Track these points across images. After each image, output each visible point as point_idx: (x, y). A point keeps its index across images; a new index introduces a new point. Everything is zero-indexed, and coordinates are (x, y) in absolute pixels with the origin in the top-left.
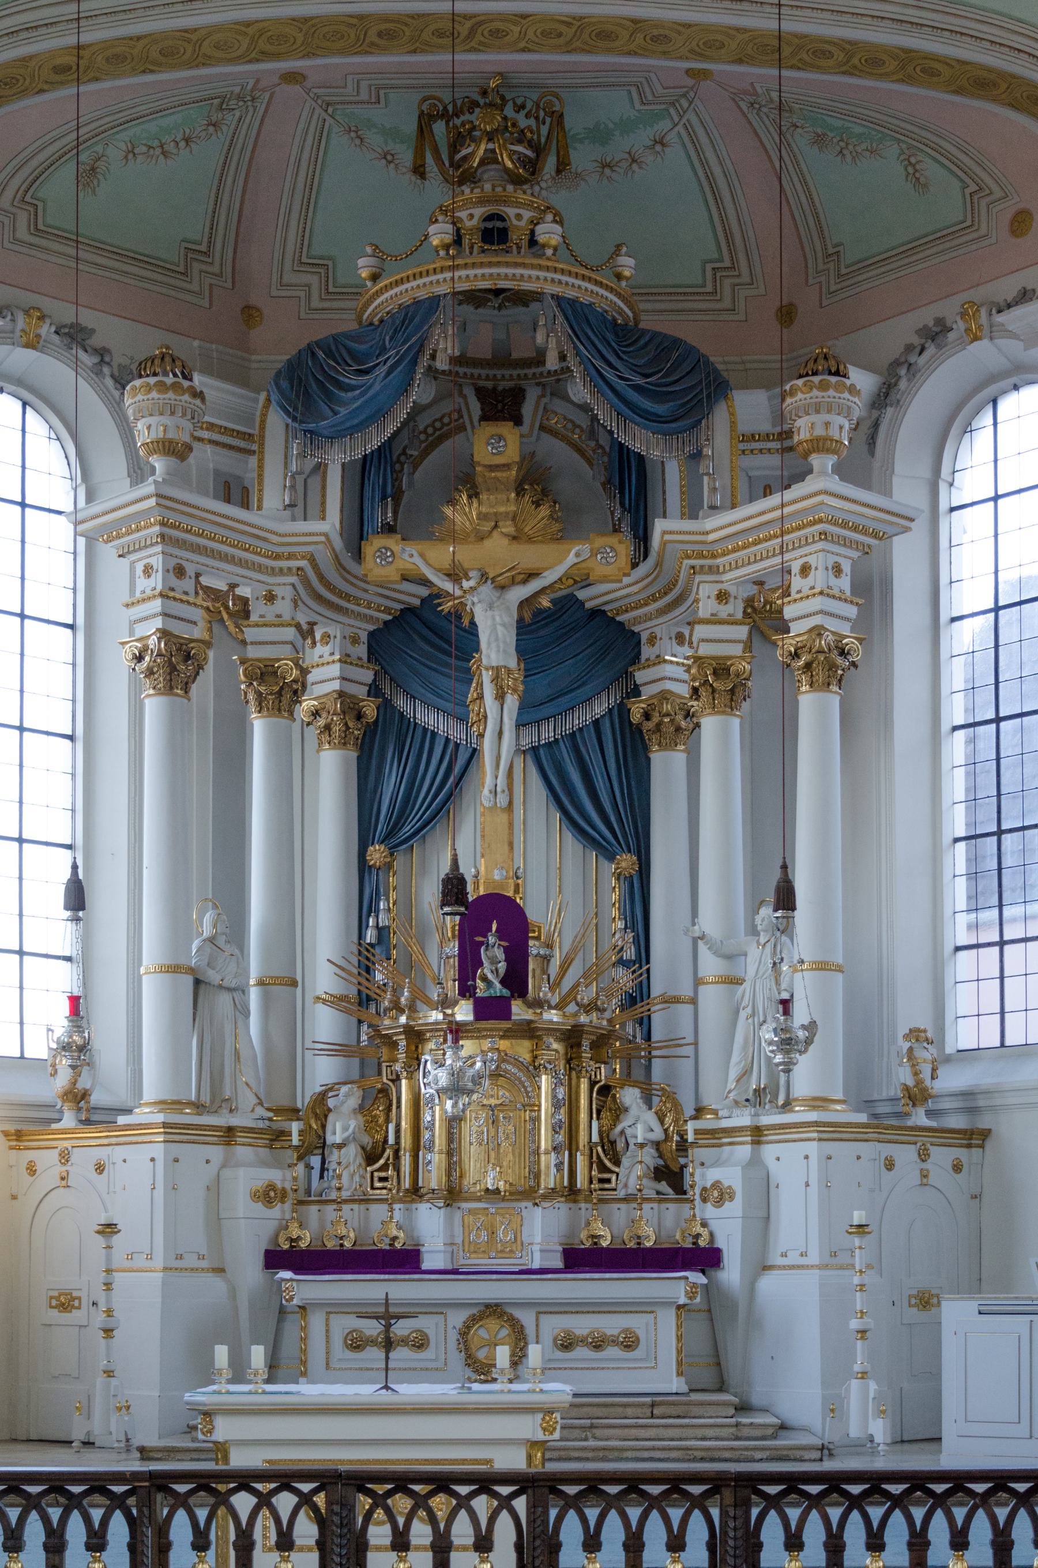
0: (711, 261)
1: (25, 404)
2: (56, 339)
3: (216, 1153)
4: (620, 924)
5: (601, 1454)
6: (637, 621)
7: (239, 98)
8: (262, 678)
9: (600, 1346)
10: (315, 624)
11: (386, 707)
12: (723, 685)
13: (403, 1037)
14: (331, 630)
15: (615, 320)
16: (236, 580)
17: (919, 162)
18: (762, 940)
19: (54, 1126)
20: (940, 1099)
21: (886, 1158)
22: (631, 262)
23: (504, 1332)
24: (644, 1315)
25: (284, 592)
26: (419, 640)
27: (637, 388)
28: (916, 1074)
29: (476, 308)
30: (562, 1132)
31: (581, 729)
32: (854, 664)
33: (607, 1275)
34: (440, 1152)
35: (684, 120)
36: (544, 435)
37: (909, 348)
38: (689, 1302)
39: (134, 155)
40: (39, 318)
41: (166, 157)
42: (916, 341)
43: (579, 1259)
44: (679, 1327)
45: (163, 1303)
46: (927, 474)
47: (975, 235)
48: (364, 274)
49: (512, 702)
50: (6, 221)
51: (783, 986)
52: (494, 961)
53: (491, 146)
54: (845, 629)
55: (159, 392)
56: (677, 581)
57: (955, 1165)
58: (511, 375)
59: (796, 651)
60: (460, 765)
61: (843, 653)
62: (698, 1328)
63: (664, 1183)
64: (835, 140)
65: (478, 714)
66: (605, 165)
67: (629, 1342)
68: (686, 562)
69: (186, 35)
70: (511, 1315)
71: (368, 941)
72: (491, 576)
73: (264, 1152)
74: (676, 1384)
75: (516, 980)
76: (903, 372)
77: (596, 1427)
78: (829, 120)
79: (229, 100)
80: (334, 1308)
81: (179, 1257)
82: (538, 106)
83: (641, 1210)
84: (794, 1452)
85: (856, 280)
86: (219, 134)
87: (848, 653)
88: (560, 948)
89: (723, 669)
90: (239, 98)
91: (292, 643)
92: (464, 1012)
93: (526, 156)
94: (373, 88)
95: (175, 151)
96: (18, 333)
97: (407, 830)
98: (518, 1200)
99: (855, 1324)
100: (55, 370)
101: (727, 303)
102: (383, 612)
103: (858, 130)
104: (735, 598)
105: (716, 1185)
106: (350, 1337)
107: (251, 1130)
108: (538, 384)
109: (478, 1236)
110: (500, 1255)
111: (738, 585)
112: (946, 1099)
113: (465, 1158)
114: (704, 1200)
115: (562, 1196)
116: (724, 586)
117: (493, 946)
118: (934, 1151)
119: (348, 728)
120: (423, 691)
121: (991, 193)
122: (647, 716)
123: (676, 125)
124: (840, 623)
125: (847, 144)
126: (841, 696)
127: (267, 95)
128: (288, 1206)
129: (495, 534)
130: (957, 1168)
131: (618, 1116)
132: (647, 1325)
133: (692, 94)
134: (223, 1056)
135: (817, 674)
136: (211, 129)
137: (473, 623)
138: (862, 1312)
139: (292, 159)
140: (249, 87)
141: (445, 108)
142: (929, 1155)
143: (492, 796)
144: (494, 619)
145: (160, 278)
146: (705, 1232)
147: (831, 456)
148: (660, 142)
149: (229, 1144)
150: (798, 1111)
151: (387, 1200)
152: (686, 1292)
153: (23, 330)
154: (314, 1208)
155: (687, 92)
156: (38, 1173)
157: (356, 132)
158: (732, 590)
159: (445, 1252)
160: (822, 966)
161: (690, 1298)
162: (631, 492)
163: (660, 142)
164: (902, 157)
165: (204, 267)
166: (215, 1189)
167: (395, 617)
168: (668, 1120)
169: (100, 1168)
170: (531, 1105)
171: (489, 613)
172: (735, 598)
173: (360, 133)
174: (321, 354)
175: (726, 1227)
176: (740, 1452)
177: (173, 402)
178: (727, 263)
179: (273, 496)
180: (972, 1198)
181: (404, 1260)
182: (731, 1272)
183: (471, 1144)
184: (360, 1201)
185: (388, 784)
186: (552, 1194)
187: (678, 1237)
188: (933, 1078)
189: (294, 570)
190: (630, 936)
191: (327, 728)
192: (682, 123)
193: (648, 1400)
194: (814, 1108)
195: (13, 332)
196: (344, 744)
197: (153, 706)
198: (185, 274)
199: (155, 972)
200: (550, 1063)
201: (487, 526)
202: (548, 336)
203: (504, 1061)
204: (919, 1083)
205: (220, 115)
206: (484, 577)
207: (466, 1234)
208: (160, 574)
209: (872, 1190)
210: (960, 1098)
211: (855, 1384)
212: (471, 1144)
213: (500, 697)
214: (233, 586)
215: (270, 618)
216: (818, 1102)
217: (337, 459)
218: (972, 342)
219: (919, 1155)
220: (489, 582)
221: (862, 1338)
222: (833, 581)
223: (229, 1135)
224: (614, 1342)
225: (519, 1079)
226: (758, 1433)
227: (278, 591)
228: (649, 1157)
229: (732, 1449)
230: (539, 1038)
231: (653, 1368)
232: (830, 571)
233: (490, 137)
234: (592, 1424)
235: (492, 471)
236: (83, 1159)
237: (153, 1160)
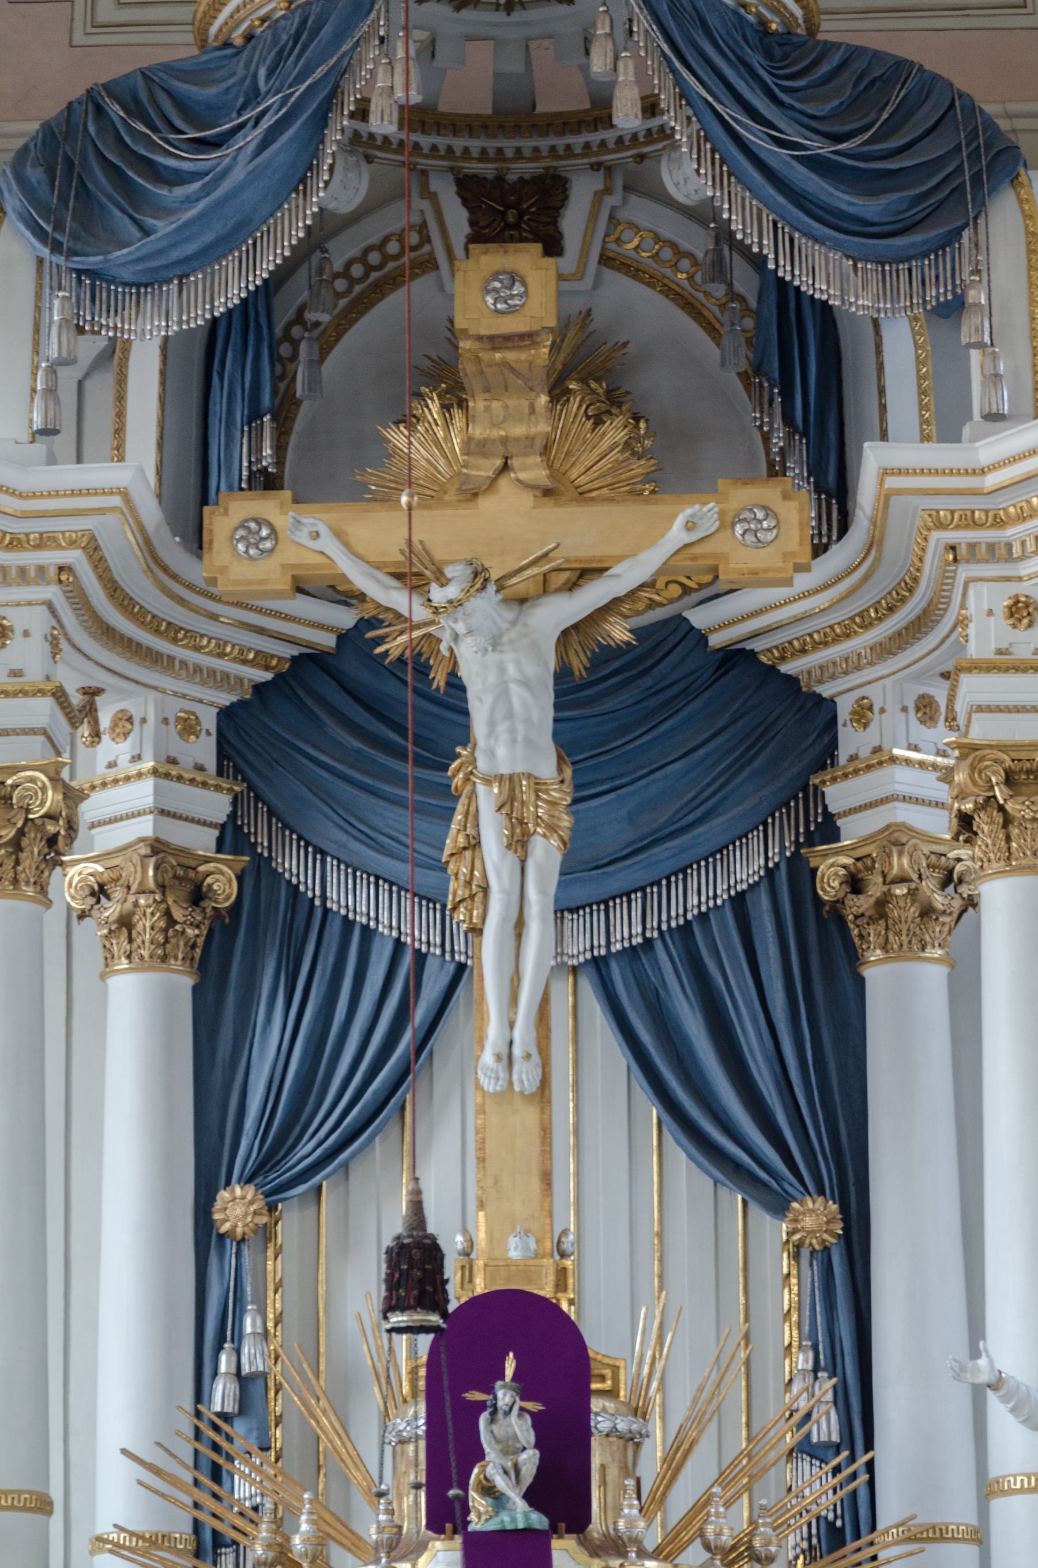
4: (803, 1361)
11: (258, 874)
26: (331, 724)
29: (458, 9)
31: (703, 917)
36: (609, 274)
49: (546, 853)
52: (510, 1448)
56: (916, 580)
60: (427, 1000)
65: (469, 883)
91: (45, 732)
97: (307, 1150)
102: (252, 663)
108: (596, 167)
117: (508, 1413)
119: (171, 922)
122: (855, 884)
129: (503, 483)
137: (456, 686)
162: (806, 393)
167: (279, 676)
171: (492, 657)
174: (116, 110)
185: (263, 1050)
189: (52, 572)
190: (826, 1385)
191: (125, 923)
206: (479, 577)
213: (519, 843)
217: (148, 336)
220: (492, 588)
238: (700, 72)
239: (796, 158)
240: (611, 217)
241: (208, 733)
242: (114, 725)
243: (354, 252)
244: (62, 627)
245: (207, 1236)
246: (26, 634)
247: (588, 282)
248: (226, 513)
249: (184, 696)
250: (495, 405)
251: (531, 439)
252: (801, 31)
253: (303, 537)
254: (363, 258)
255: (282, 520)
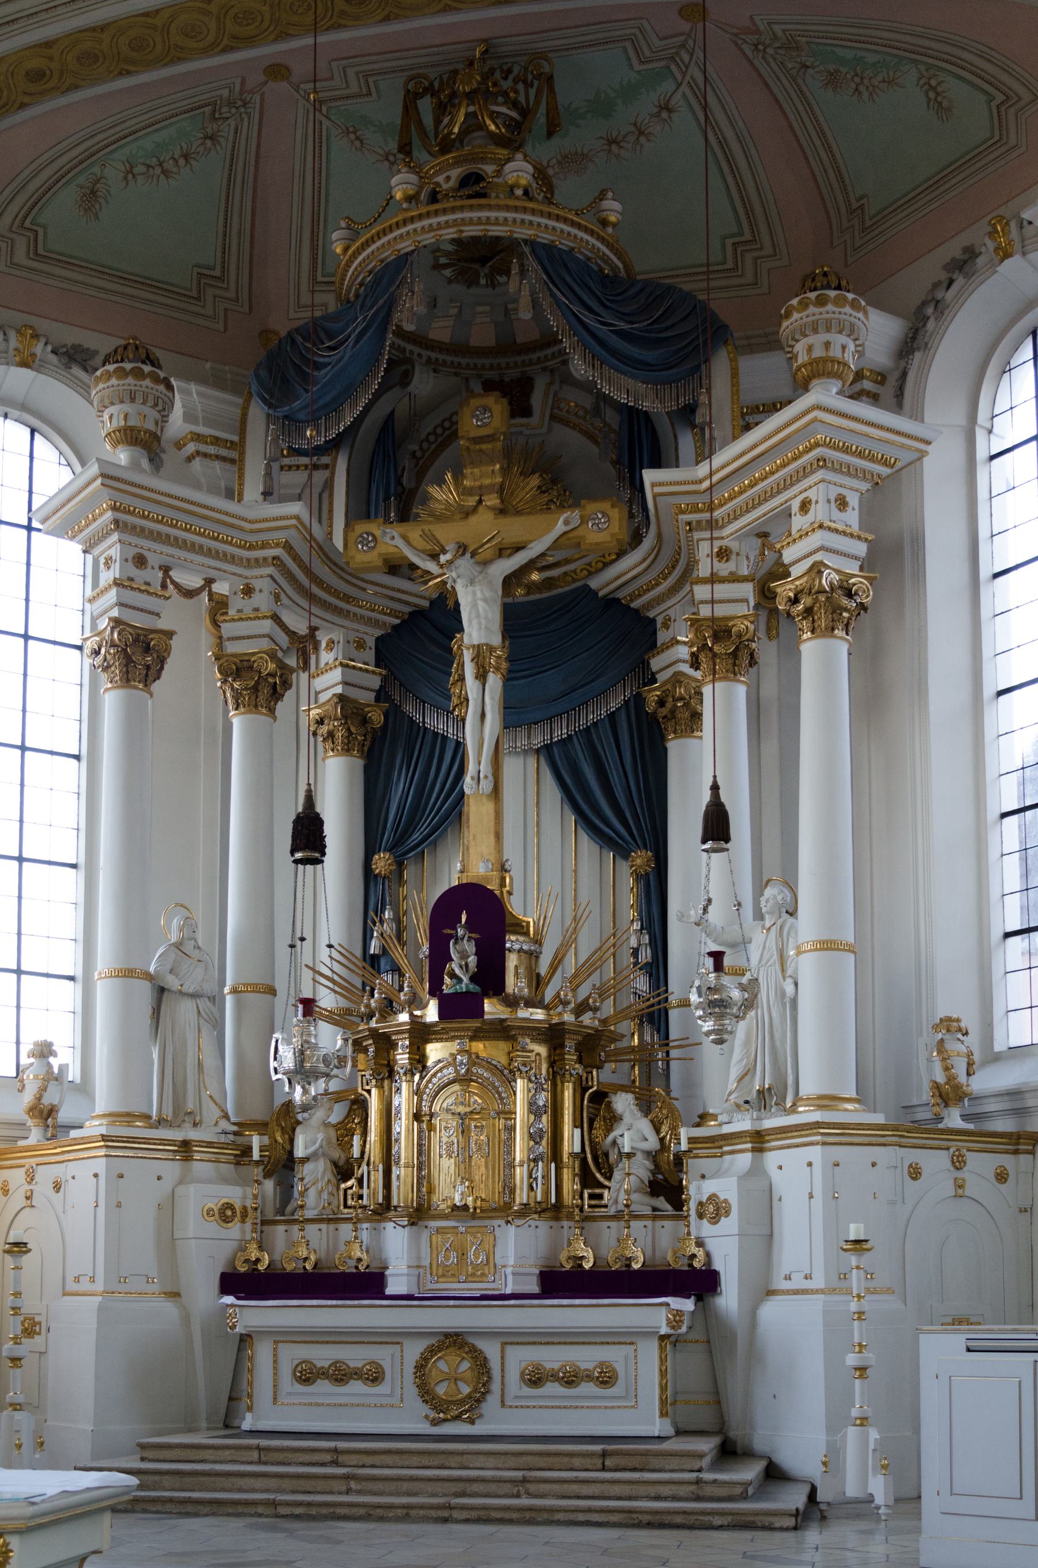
0: (733, 236)
1: (33, 432)
2: (53, 358)
3: (172, 1169)
4: (636, 926)
5: (527, 1515)
6: (650, 605)
7: (231, 104)
8: (238, 674)
9: (573, 1381)
10: (316, 629)
11: (394, 713)
12: (727, 650)
13: (371, 1042)
14: (334, 636)
15: (601, 270)
16: (213, 574)
17: (940, 83)
18: (768, 924)
19: (21, 1143)
20: (986, 1101)
21: (911, 1166)
22: (617, 206)
23: (466, 1365)
24: (623, 1346)
25: (263, 585)
26: (416, 642)
27: (621, 334)
28: (947, 1069)
29: (469, 287)
30: (544, 1142)
31: (595, 724)
32: (862, 607)
33: (577, 1302)
34: (407, 1166)
35: (688, 78)
36: (555, 425)
37: (936, 285)
38: (672, 1332)
39: (134, 176)
40: (32, 337)
41: (167, 177)
42: (943, 276)
43: (559, 1282)
44: (663, 1361)
45: (98, 1329)
46: (961, 420)
47: (1003, 149)
48: (338, 250)
49: (494, 681)
50: (3, 245)
51: (789, 972)
52: (464, 956)
53: (471, 109)
54: (852, 568)
55: (118, 378)
56: (680, 548)
57: (998, 1174)
58: (516, 363)
59: (796, 595)
61: (850, 594)
62: (692, 1365)
63: (662, 1198)
64: (849, 76)
65: (460, 697)
66: (612, 142)
67: (606, 1378)
68: (681, 517)
69: (149, 20)
70: (473, 1345)
71: (372, 952)
72: (471, 549)
73: (228, 1169)
74: (658, 1426)
75: (490, 977)
76: (930, 310)
77: (529, 1482)
78: (840, 52)
79: (220, 108)
80: (282, 1336)
81: (123, 1280)
82: (526, 69)
83: (628, 1227)
84: (762, 1518)
85: (879, 229)
86: (218, 147)
87: (856, 594)
88: (576, 954)
89: (724, 631)
90: (231, 104)
91: (269, 636)
92: (431, 1013)
93: (511, 118)
94: (360, 76)
95: (175, 170)
96: (11, 352)
97: (416, 837)
98: (491, 1218)
99: (852, 1359)
100: (50, 389)
101: (749, 278)
102: (389, 615)
103: (871, 58)
104: (738, 554)
105: (712, 1198)
106: (299, 1368)
107: (210, 1144)
108: (544, 369)
109: (447, 1258)
110: (470, 1279)
111: (739, 539)
112: (992, 1100)
113: (435, 1172)
114: (701, 1216)
115: (536, 1213)
116: (725, 543)
117: (462, 939)
118: (970, 1157)
119: (350, 733)
120: (433, 695)
121: (1020, 99)
122: (661, 703)
123: (681, 84)
124: (844, 561)
125: (862, 79)
126: (850, 644)
127: (257, 98)
128: (248, 1226)
129: (481, 509)
130: (1002, 1177)
131: (612, 1126)
132: (626, 1358)
133: (691, 42)
134: (185, 1068)
135: (819, 619)
136: (209, 143)
137: (457, 604)
138: (860, 1345)
139: (297, 173)
140: (237, 88)
141: (431, 84)
142: (965, 1163)
143: (474, 784)
144: (474, 593)
145: (176, 303)
146: (700, 1253)
147: (833, 381)
148: (666, 107)
149: (186, 1160)
150: (801, 1112)
151: (351, 1219)
152: (668, 1319)
153: (16, 349)
154: (281, 1228)
155: (686, 41)
156: (10, 1192)
157: (355, 133)
158: (734, 545)
159: (408, 1275)
160: (827, 946)
161: (673, 1327)
163: (666, 107)
164: (922, 82)
165: (217, 292)
166: (168, 1210)
167: (403, 622)
168: (664, 1129)
169: (57, 1187)
170: (506, 1113)
171: (470, 588)
172: (738, 554)
173: (359, 133)
174: (299, 339)
175: (723, 1246)
176: (695, 1517)
177: (133, 388)
178: (748, 236)
179: (253, 488)
180: (1021, 1211)
181: (367, 1284)
182: (729, 1299)
183: (441, 1156)
184: (329, 1221)
185: (396, 791)
186: (526, 1211)
187: (670, 1258)
188: (969, 1074)
189: (270, 560)
190: (646, 939)
191: (331, 735)
192: (685, 82)
193: (598, 1448)
194: (821, 1107)
195: (6, 352)
196: (347, 750)
197: (112, 700)
198: (198, 299)
199: (106, 977)
200: (524, 1065)
201: (472, 501)
202: (521, 283)
203: (475, 1064)
204: (951, 1079)
205: (215, 126)
207: (434, 1256)
208: (118, 564)
209: (892, 1203)
210: (1006, 1098)
211: (852, 1432)
212: (441, 1156)
213: (482, 676)
214: (209, 582)
215: (248, 611)
216: (827, 1101)
218: (1002, 261)
219: (953, 1162)
220: (468, 555)
221: (861, 1377)
222: (836, 514)
223: (185, 1148)
224: (589, 1378)
225: (493, 1084)
226: (723, 1492)
227: (257, 584)
228: (641, 1169)
229: (685, 1512)
230: (516, 1040)
231: (633, 1407)
232: (833, 505)
233: (471, 97)
234: (524, 1477)
235: (476, 443)
236: (45, 1175)
237: (96, 1175)
238: (557, 282)
239: (611, 331)
240: (555, 396)
241: (370, 648)
242: (327, 645)
243: (438, 421)
244: (280, 587)
245: (369, 876)
246: (261, 591)
247: (545, 430)
248: (353, 530)
249: (358, 631)
250: (476, 471)
251: (492, 486)
252: (623, 273)
253: (388, 540)
254: (441, 425)
255: (378, 533)
